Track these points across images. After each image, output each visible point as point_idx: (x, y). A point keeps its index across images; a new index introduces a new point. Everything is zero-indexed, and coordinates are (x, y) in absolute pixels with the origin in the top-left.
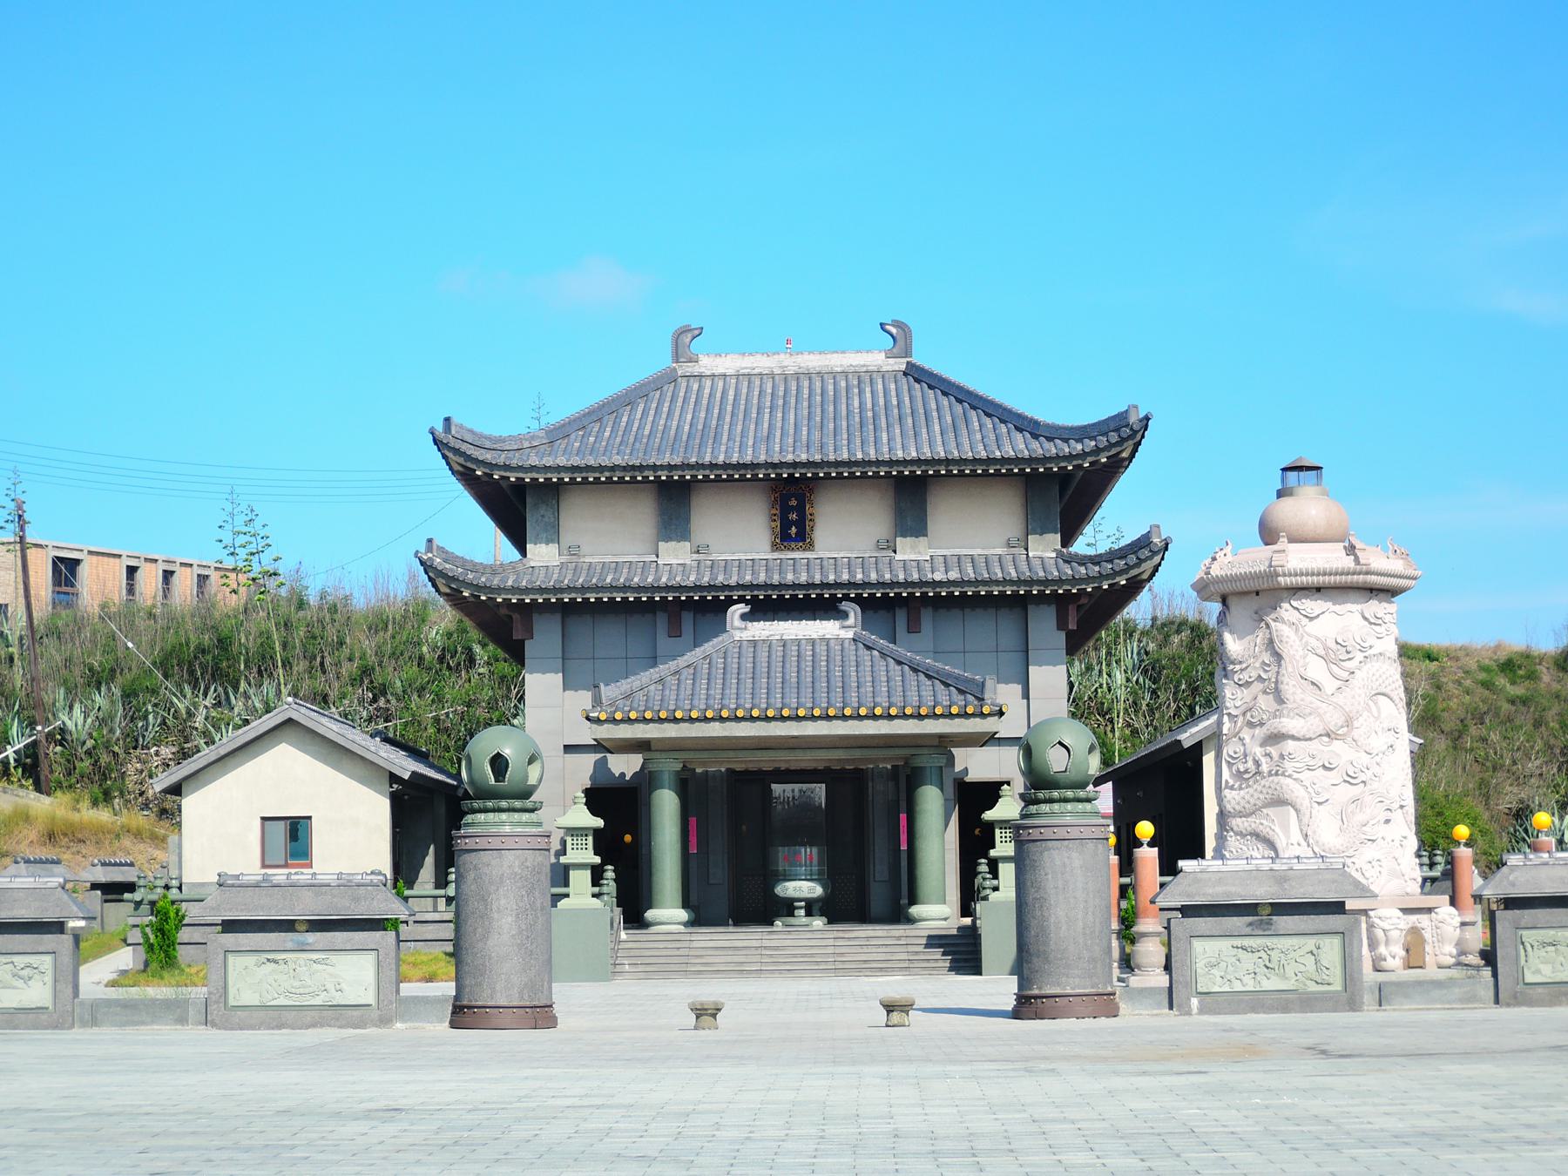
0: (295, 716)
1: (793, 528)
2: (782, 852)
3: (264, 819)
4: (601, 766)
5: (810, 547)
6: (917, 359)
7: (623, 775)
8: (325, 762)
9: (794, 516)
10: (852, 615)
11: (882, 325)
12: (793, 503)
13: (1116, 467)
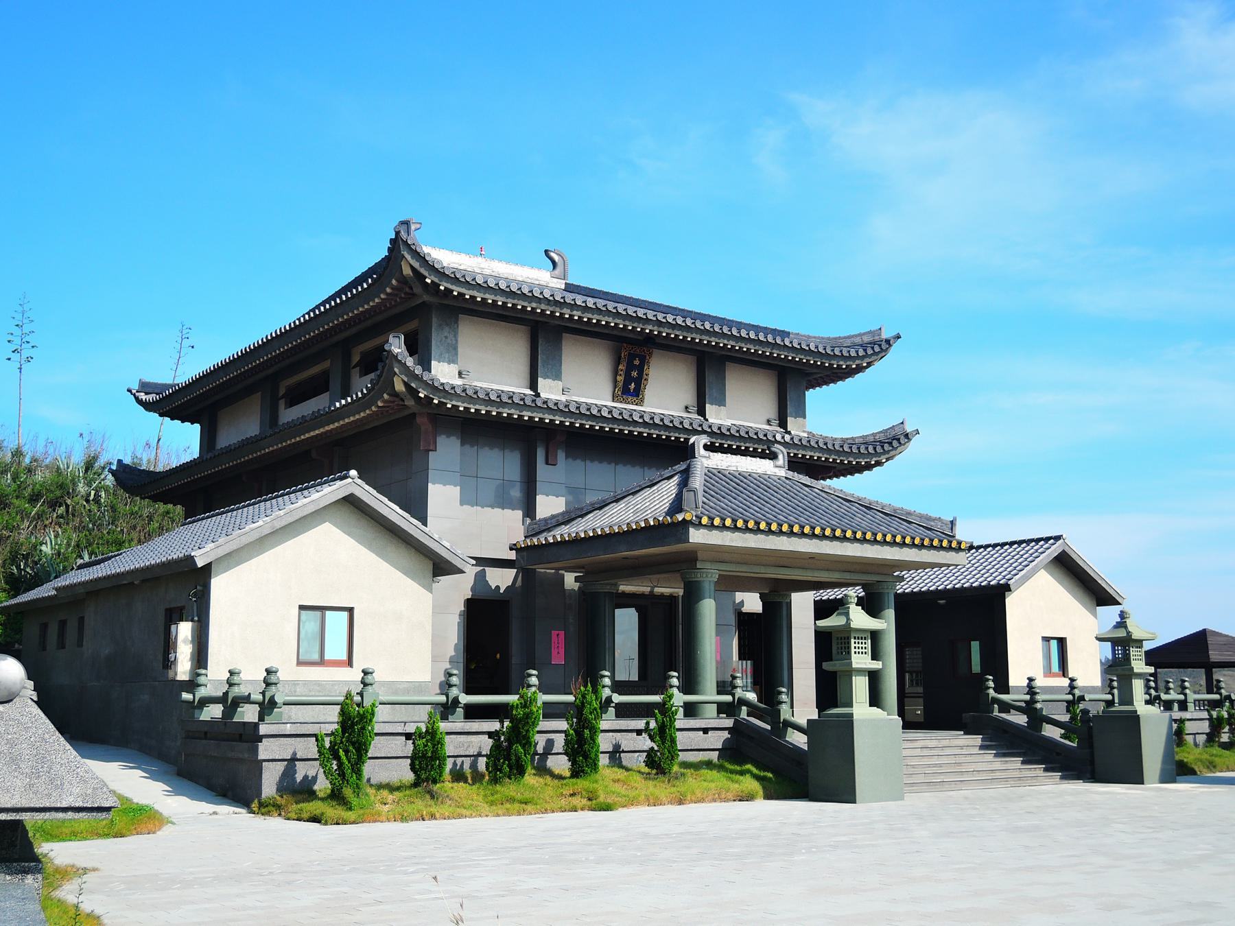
0: (359, 493)
1: (630, 384)
2: (171, 674)
3: (302, 608)
4: (480, 577)
5: (641, 403)
6: (573, 280)
7: (498, 587)
8: (370, 548)
9: (635, 374)
10: (780, 457)
11: (546, 251)
12: (637, 362)
13: (850, 373)
